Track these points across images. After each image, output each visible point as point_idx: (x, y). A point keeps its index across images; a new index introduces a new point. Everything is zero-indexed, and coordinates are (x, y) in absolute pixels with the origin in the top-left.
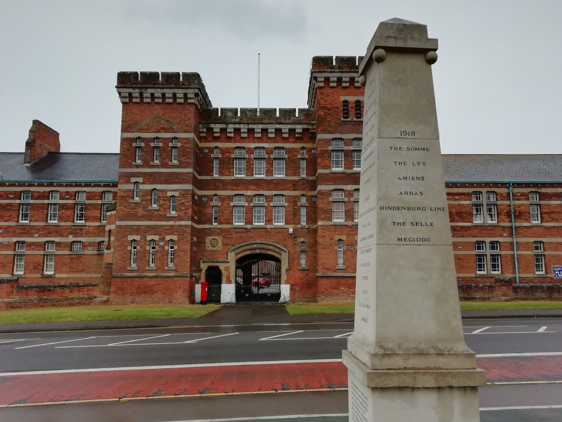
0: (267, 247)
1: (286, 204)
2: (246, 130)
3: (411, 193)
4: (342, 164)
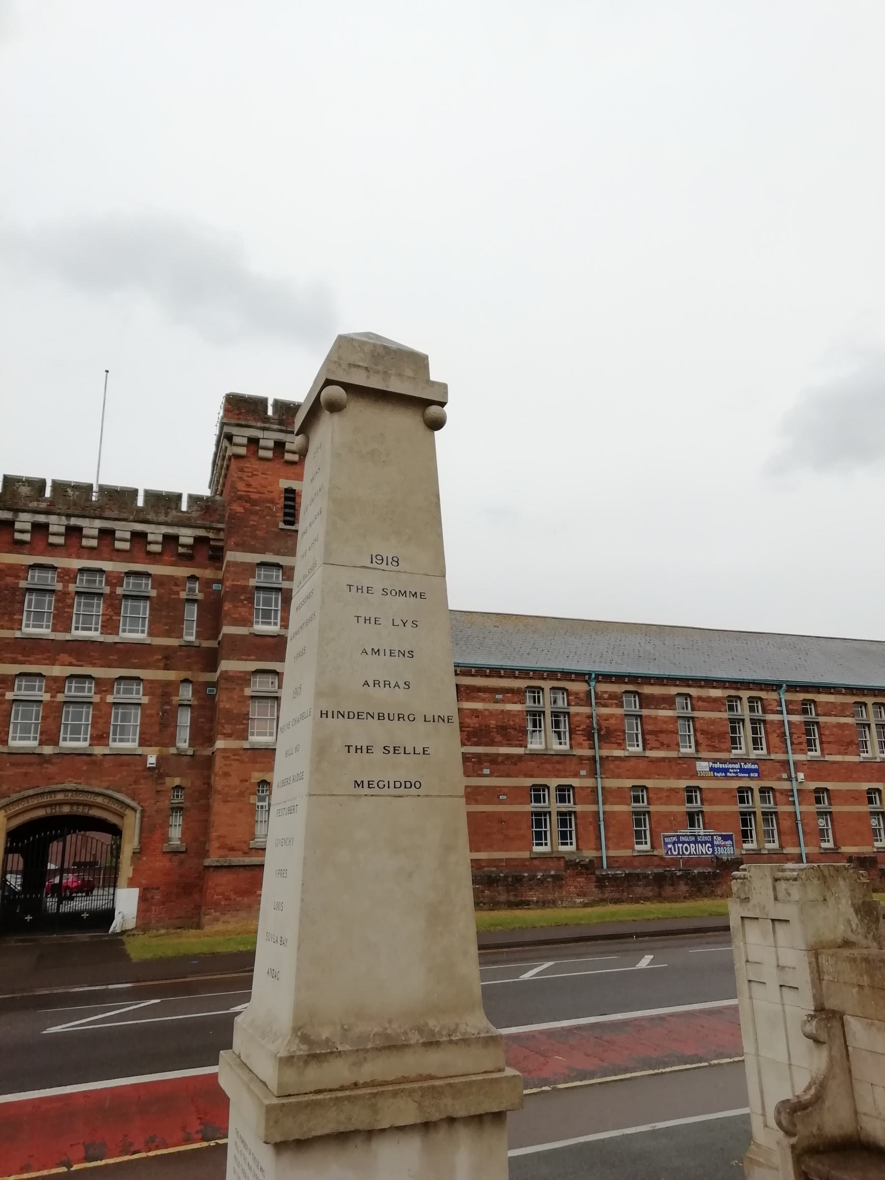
0: (90, 799)
1: (145, 700)
2: (62, 530)
3: (387, 684)
4: (276, 618)
